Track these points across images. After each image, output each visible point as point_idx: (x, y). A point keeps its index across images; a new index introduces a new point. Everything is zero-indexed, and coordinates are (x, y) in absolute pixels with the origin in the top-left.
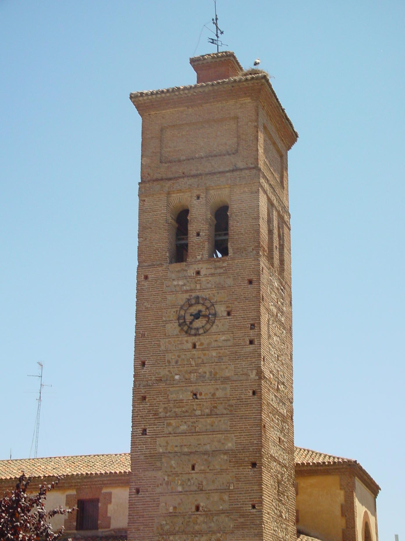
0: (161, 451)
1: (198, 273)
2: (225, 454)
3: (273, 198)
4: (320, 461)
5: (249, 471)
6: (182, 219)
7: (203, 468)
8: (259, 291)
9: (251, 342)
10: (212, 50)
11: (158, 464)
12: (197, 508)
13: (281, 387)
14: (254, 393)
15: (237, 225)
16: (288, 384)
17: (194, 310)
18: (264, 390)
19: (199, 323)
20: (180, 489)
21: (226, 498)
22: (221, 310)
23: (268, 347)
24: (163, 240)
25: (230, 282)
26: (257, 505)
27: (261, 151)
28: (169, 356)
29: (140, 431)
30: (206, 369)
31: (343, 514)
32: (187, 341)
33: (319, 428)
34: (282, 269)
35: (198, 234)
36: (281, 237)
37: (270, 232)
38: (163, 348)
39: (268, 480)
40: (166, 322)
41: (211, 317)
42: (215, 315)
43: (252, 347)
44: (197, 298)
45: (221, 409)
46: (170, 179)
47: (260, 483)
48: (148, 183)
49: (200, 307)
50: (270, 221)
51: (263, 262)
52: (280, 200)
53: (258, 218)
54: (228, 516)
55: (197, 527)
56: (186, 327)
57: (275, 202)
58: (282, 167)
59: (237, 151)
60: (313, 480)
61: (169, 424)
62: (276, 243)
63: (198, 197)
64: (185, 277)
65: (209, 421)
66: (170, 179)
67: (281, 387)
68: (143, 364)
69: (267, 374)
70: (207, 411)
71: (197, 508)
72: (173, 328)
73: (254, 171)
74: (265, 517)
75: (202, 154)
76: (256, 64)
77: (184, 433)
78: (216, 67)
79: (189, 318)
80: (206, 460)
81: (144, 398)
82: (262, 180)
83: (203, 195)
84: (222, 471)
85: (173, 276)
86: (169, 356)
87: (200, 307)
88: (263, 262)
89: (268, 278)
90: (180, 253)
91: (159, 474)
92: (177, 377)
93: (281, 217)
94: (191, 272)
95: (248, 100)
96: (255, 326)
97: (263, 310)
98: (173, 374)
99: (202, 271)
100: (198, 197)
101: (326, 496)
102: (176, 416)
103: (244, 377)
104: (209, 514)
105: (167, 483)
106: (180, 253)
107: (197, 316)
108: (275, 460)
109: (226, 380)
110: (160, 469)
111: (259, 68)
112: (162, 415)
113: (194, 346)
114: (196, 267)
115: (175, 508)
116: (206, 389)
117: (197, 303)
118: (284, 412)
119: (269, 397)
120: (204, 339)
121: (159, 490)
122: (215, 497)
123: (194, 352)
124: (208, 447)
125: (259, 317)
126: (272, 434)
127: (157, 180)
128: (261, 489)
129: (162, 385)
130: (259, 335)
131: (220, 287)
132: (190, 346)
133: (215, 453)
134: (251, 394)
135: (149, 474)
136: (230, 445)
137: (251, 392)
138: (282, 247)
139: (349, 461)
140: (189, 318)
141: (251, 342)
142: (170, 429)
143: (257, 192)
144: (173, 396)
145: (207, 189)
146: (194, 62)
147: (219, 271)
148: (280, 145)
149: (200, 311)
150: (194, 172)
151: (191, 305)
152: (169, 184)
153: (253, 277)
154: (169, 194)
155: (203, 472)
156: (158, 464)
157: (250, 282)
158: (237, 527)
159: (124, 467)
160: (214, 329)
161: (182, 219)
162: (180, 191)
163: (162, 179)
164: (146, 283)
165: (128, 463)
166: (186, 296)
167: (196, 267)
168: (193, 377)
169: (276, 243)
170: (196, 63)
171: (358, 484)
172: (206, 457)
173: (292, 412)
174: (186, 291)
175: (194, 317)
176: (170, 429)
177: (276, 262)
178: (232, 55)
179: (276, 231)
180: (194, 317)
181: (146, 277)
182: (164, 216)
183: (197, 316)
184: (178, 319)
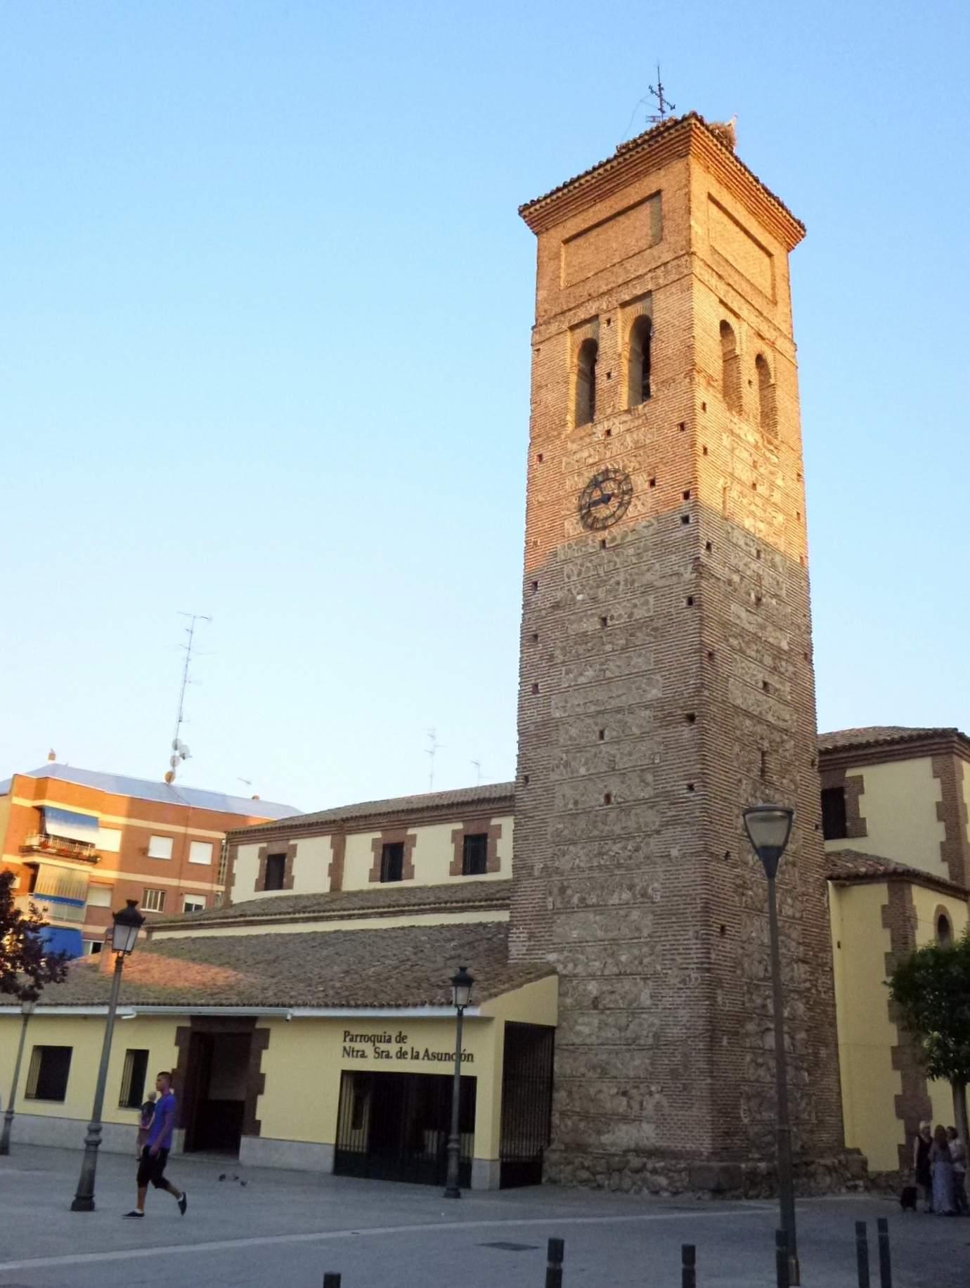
0: (558, 715)
1: (608, 433)
2: (646, 707)
7: (615, 734)
12: (608, 797)
14: (690, 601)
21: (649, 778)
22: (640, 482)
40: (565, 518)
43: (686, 529)
51: (703, 394)
54: (651, 808)
71: (608, 797)
80: (620, 721)
84: (641, 738)
85: (575, 447)
90: (588, 411)
92: (580, 597)
98: (574, 592)
103: (675, 579)
104: (625, 809)
106: (588, 411)
111: (58, 761)
115: (576, 803)
121: (554, 776)
134: (685, 604)
136: (655, 693)
137: (685, 601)
141: (686, 520)
146: (523, 210)
150: (604, 288)
167: (606, 425)
170: (526, 213)
172: (620, 716)
184: (580, 509)
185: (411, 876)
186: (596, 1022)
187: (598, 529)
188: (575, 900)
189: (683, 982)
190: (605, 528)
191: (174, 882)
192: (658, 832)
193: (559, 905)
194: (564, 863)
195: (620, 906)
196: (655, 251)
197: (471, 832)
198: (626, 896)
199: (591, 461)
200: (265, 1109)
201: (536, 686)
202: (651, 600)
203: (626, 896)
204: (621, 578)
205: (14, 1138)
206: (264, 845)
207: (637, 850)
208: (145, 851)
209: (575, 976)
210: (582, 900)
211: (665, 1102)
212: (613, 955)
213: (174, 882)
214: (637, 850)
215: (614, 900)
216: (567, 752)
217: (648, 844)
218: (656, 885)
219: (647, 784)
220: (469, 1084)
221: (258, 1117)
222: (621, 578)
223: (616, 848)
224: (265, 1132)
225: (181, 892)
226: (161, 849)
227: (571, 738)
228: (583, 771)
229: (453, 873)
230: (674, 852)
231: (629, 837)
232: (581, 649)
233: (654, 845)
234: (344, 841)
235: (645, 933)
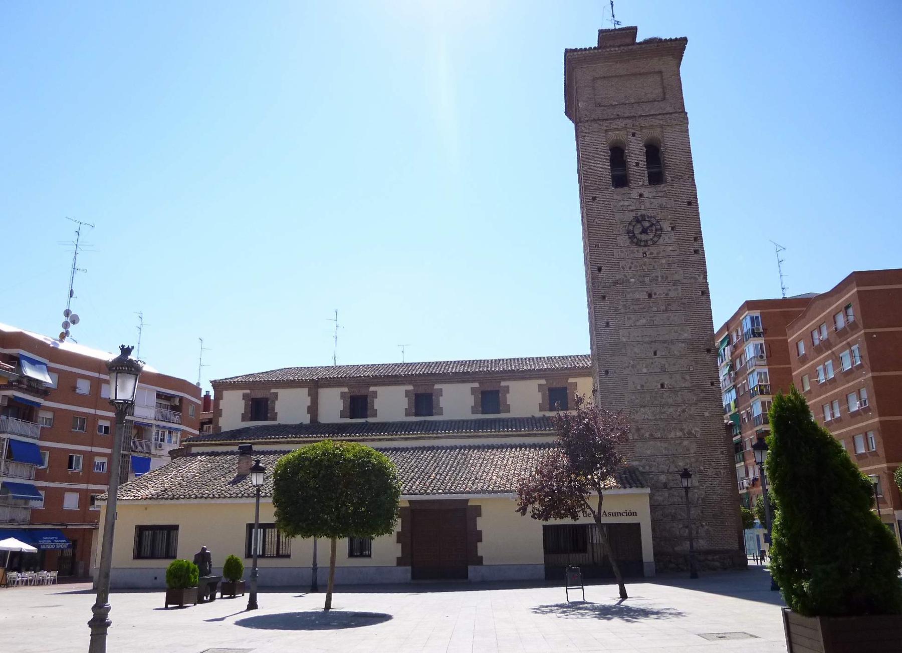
12: (662, 386)
21: (688, 377)
22: (666, 226)
92: (632, 280)
103: (693, 281)
104: (674, 391)
115: (642, 386)
121: (626, 372)
185: (275, 419)
186: (667, 495)
187: (640, 246)
188: (647, 435)
189: (717, 474)
190: (645, 246)
191: (92, 411)
192: (696, 404)
193: (636, 437)
194: (637, 417)
195: (676, 438)
196: (662, 104)
197: (253, 396)
198: (679, 434)
199: (631, 208)
200: (482, 549)
201: (608, 323)
202: (679, 288)
203: (679, 434)
204: (659, 274)
205: (318, 582)
206: (248, 391)
207: (684, 411)
208: (74, 388)
209: (652, 472)
210: (651, 435)
211: (710, 529)
212: (673, 462)
213: (92, 411)
214: (684, 411)
215: (672, 435)
216: (633, 360)
217: (690, 409)
218: (697, 429)
219: (686, 380)
220: (638, 525)
221: (479, 554)
222: (659, 274)
223: (671, 410)
224: (484, 563)
225: (97, 418)
226: (83, 387)
227: (635, 353)
228: (645, 370)
229: (342, 416)
230: (706, 414)
231: (678, 405)
232: (636, 307)
233: (693, 410)
234: (317, 393)
235: (692, 451)
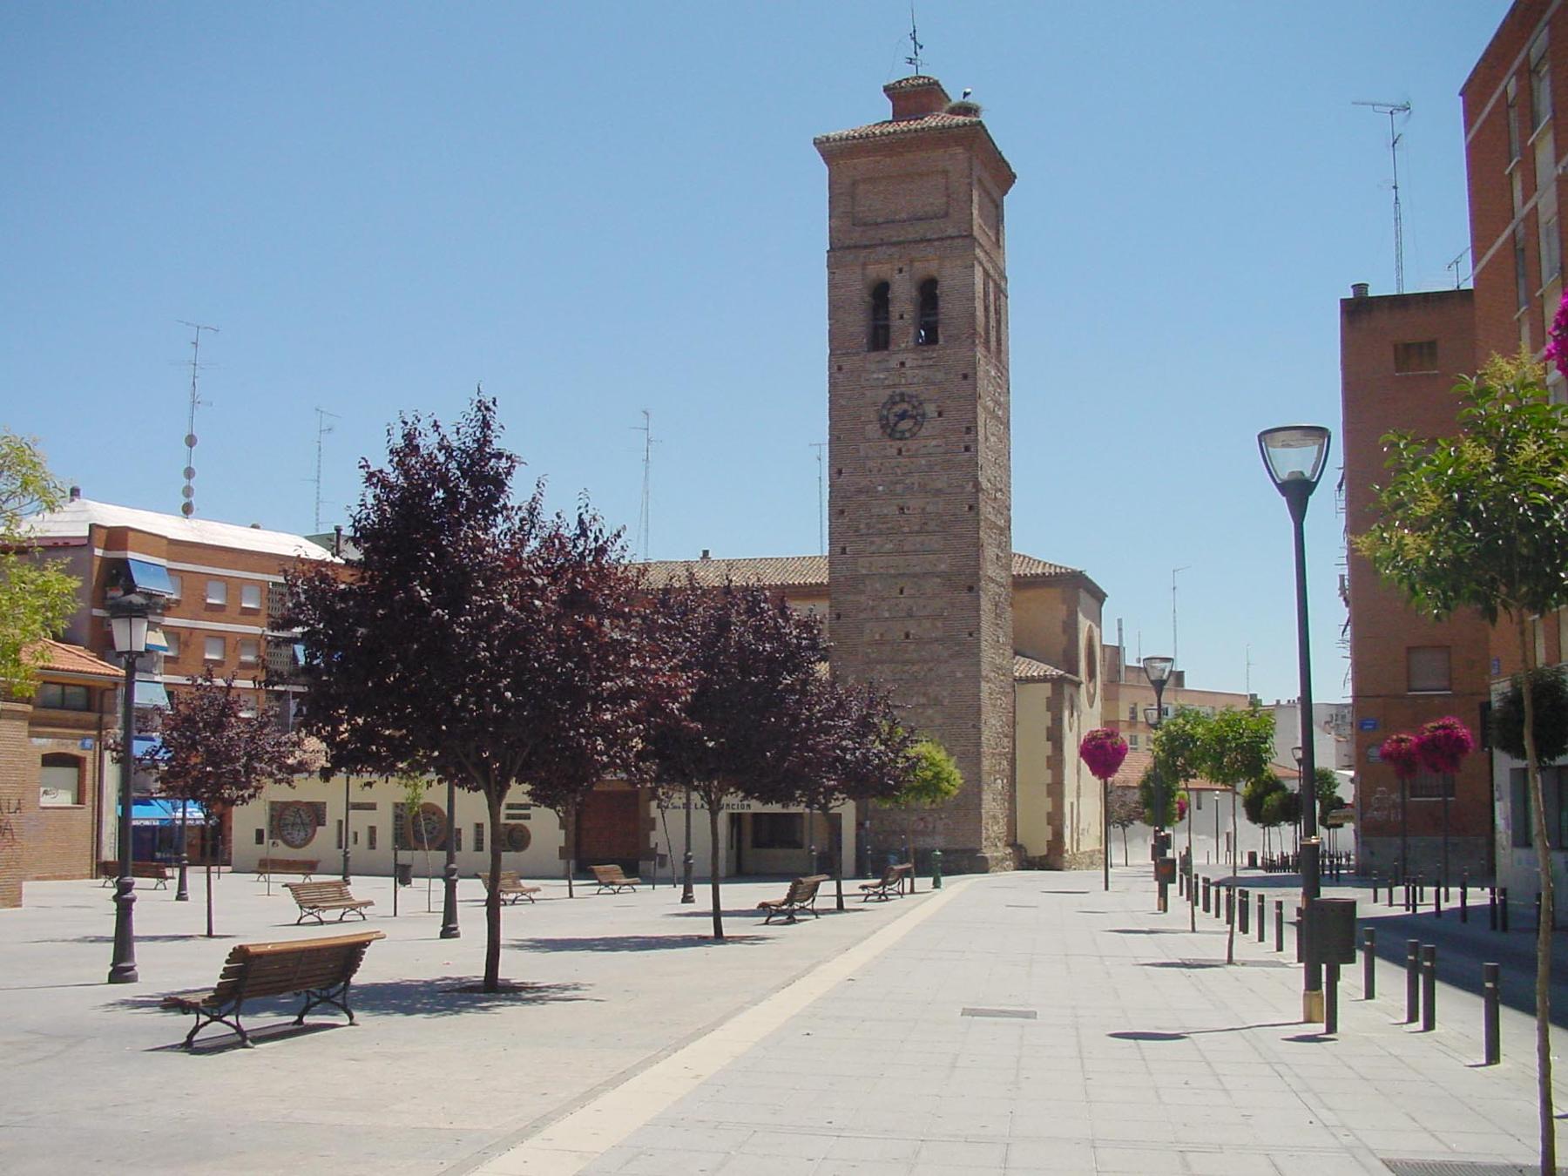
1: (903, 364)
3: (989, 266)
4: (1039, 571)
5: (965, 596)
6: (880, 294)
8: (975, 388)
9: (967, 449)
10: (908, 72)
11: (861, 586)
12: (907, 636)
13: (999, 495)
14: (971, 508)
15: (949, 307)
16: (1005, 489)
17: (898, 409)
18: (982, 504)
19: (905, 425)
20: (887, 615)
21: (939, 625)
22: (930, 409)
23: (985, 455)
24: (858, 323)
25: (940, 376)
26: (974, 632)
27: (975, 212)
28: (870, 464)
29: (836, 537)
30: (915, 479)
31: (1064, 631)
32: (891, 447)
33: (1039, 532)
34: (998, 353)
35: (901, 317)
36: (998, 312)
37: (986, 309)
38: (862, 453)
39: (986, 604)
41: (919, 419)
42: (924, 415)
44: (902, 394)
45: (932, 526)
46: (866, 247)
47: (978, 609)
48: (840, 251)
49: (905, 406)
50: (986, 294)
51: (980, 352)
52: (996, 267)
53: (973, 299)
55: (907, 656)
56: (890, 430)
57: (992, 271)
58: (996, 221)
59: (946, 215)
60: (1030, 594)
61: (872, 543)
62: (993, 323)
63: (901, 271)
64: (887, 370)
65: (918, 539)
66: (866, 247)
67: (999, 495)
68: (840, 472)
69: (985, 484)
70: (916, 528)
71: (907, 636)
72: (873, 430)
73: (968, 241)
74: (983, 644)
75: (904, 216)
76: (966, 94)
77: (889, 553)
78: (914, 97)
79: (892, 419)
81: (842, 512)
82: (978, 251)
83: (905, 269)
86: (870, 464)
87: (905, 406)
88: (980, 352)
89: (985, 369)
90: (879, 339)
91: (863, 598)
93: (997, 286)
94: (894, 363)
95: (960, 150)
96: (971, 429)
97: (980, 409)
99: (906, 365)
100: (901, 271)
101: (1046, 610)
102: (880, 534)
105: (873, 608)
106: (879, 339)
107: (903, 416)
108: (993, 580)
109: (938, 492)
110: (862, 592)
112: (864, 531)
113: (900, 452)
114: (901, 357)
116: (914, 503)
117: (903, 401)
118: (1002, 523)
119: (987, 510)
120: (912, 445)
121: (862, 616)
122: (927, 624)
123: (900, 459)
124: (917, 569)
125: (975, 418)
126: (990, 552)
127: (848, 248)
128: (979, 616)
129: (863, 497)
130: (976, 440)
131: (928, 382)
132: (895, 452)
133: (925, 575)
135: (850, 597)
138: (999, 322)
139: (1074, 572)
140: (892, 419)
142: (873, 548)
143: (973, 266)
144: (875, 511)
145: (912, 261)
147: (927, 362)
148: (995, 195)
149: (905, 411)
151: (894, 403)
152: (863, 253)
153: (969, 371)
154: (864, 265)
155: (912, 596)
156: (861, 586)
157: (965, 377)
158: (951, 656)
159: (824, 578)
160: (923, 432)
161: (880, 294)
162: (878, 262)
163: (855, 247)
164: (840, 376)
165: (825, 565)
166: (889, 392)
168: (899, 488)
169: (993, 323)
171: (1083, 595)
173: (1009, 521)
174: (889, 386)
175: (899, 418)
176: (873, 548)
177: (993, 344)
178: (936, 83)
179: (992, 308)
180: (899, 418)
181: (840, 369)
182: (858, 291)
183: (903, 416)
